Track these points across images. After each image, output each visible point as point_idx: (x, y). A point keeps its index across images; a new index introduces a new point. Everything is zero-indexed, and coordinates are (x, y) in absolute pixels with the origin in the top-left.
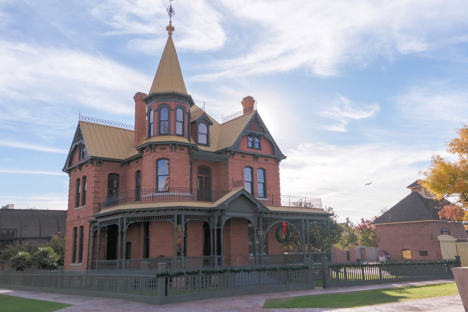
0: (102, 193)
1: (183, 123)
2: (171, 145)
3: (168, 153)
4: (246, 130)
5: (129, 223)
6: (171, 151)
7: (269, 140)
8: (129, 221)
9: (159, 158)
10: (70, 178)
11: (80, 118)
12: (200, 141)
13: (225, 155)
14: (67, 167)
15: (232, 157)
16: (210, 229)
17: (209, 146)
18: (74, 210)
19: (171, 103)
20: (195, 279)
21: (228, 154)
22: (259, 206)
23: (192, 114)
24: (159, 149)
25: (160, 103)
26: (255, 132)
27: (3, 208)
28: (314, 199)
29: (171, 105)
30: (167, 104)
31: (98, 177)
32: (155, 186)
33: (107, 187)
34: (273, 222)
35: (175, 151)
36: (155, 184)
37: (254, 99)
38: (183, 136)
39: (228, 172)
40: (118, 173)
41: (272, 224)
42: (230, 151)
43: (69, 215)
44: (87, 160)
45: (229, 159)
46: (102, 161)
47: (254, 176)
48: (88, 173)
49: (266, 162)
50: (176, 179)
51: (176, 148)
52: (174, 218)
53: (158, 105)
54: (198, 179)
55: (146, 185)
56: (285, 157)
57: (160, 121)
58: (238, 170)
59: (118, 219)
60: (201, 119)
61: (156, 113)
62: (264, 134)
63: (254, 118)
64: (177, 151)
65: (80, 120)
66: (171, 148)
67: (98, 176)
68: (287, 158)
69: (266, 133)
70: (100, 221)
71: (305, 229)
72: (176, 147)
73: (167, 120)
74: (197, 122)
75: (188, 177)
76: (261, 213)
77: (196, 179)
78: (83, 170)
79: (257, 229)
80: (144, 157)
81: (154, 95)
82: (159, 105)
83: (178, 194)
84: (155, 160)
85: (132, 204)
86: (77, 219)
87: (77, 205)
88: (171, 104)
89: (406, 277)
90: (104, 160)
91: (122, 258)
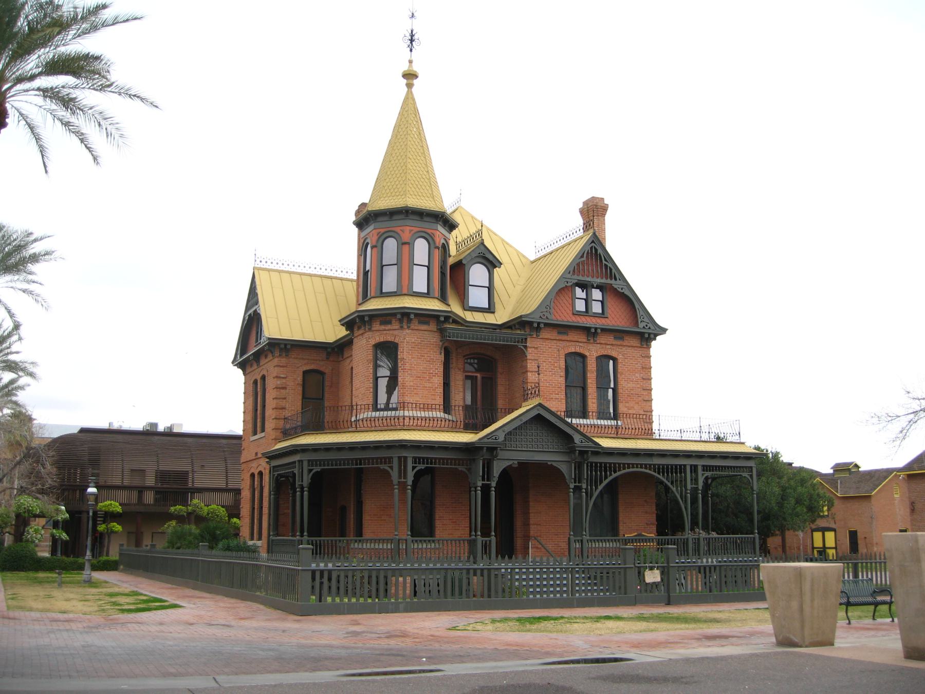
1: (428, 267)
2: (399, 316)
3: (396, 332)
4: (569, 276)
6: (402, 327)
7: (625, 295)
9: (379, 343)
11: (255, 261)
12: (472, 303)
13: (519, 332)
14: (239, 356)
15: (535, 336)
17: (492, 310)
21: (527, 330)
22: (577, 439)
25: (382, 231)
26: (589, 279)
29: (403, 232)
31: (283, 378)
32: (372, 398)
33: (300, 397)
34: (615, 472)
35: (409, 327)
36: (372, 394)
37: (581, 206)
38: (427, 295)
40: (322, 369)
41: (611, 475)
42: (530, 323)
43: (244, 449)
44: (264, 344)
45: (528, 340)
46: (289, 347)
47: (588, 373)
48: (267, 371)
50: (412, 384)
51: (409, 321)
52: (392, 463)
53: (378, 235)
54: (469, 383)
55: (357, 396)
56: (663, 331)
57: (382, 266)
58: (550, 362)
59: (294, 462)
60: (474, 255)
61: (375, 249)
62: (613, 282)
63: (588, 248)
64: (412, 327)
65: (256, 266)
66: (401, 321)
67: (282, 376)
68: (667, 332)
69: (616, 279)
70: (274, 465)
72: (411, 319)
73: (396, 263)
74: (464, 262)
75: (438, 380)
76: (582, 453)
77: (461, 383)
78: (261, 364)
79: (575, 486)
80: (355, 340)
81: (370, 215)
82: (380, 233)
84: (370, 347)
85: (319, 434)
86: (254, 458)
87: (255, 433)
89: (346, 600)
90: (292, 345)
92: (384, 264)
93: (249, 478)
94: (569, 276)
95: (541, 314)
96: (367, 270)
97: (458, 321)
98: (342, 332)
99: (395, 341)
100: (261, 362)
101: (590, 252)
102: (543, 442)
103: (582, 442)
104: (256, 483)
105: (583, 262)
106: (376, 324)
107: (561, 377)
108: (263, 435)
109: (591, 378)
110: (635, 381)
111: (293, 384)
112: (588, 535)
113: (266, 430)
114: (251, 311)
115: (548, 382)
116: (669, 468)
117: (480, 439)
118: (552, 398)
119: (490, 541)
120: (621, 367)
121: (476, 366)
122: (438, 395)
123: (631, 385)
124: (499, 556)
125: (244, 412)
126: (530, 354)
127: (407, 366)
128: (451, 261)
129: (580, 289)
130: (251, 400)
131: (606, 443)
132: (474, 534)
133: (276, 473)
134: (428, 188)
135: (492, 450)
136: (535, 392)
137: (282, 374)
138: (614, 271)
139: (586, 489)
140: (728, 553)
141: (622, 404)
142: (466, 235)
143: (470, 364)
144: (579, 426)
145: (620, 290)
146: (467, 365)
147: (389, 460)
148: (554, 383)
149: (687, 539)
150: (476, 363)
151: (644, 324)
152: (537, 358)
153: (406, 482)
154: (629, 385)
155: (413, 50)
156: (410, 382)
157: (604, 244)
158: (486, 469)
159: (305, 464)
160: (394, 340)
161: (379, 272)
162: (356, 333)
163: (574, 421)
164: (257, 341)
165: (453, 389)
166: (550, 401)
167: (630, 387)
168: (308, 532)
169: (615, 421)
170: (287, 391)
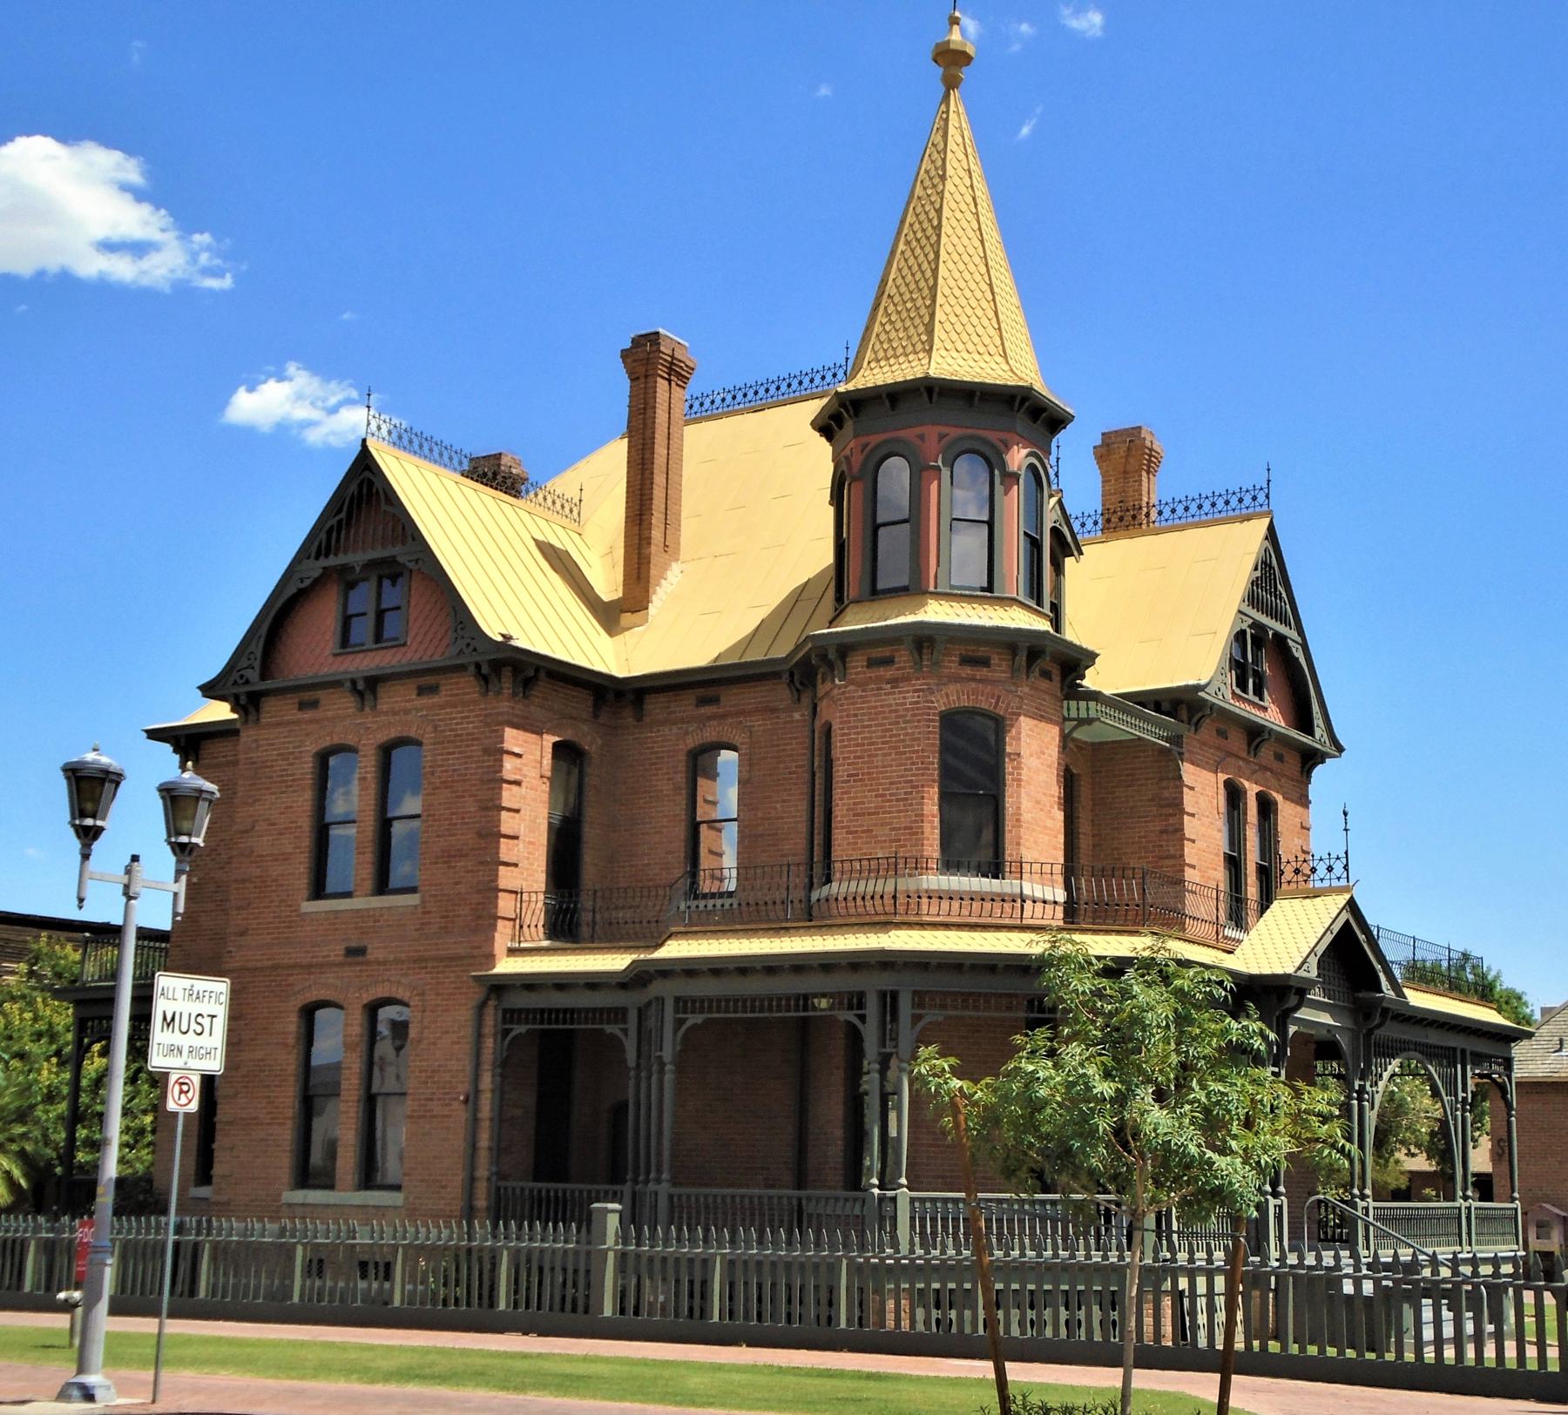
5: (512, 1030)
8: (511, 1022)
16: (672, 1076)
19: (918, 430)
25: (875, 439)
30: (898, 440)
57: (876, 528)
63: (353, 488)
82: (869, 447)
83: (890, 888)
88: (921, 437)
92: (880, 520)
99: (997, 711)
106: (949, 662)
157: (653, 572)
160: (995, 707)
161: (869, 545)
169: (500, 923)
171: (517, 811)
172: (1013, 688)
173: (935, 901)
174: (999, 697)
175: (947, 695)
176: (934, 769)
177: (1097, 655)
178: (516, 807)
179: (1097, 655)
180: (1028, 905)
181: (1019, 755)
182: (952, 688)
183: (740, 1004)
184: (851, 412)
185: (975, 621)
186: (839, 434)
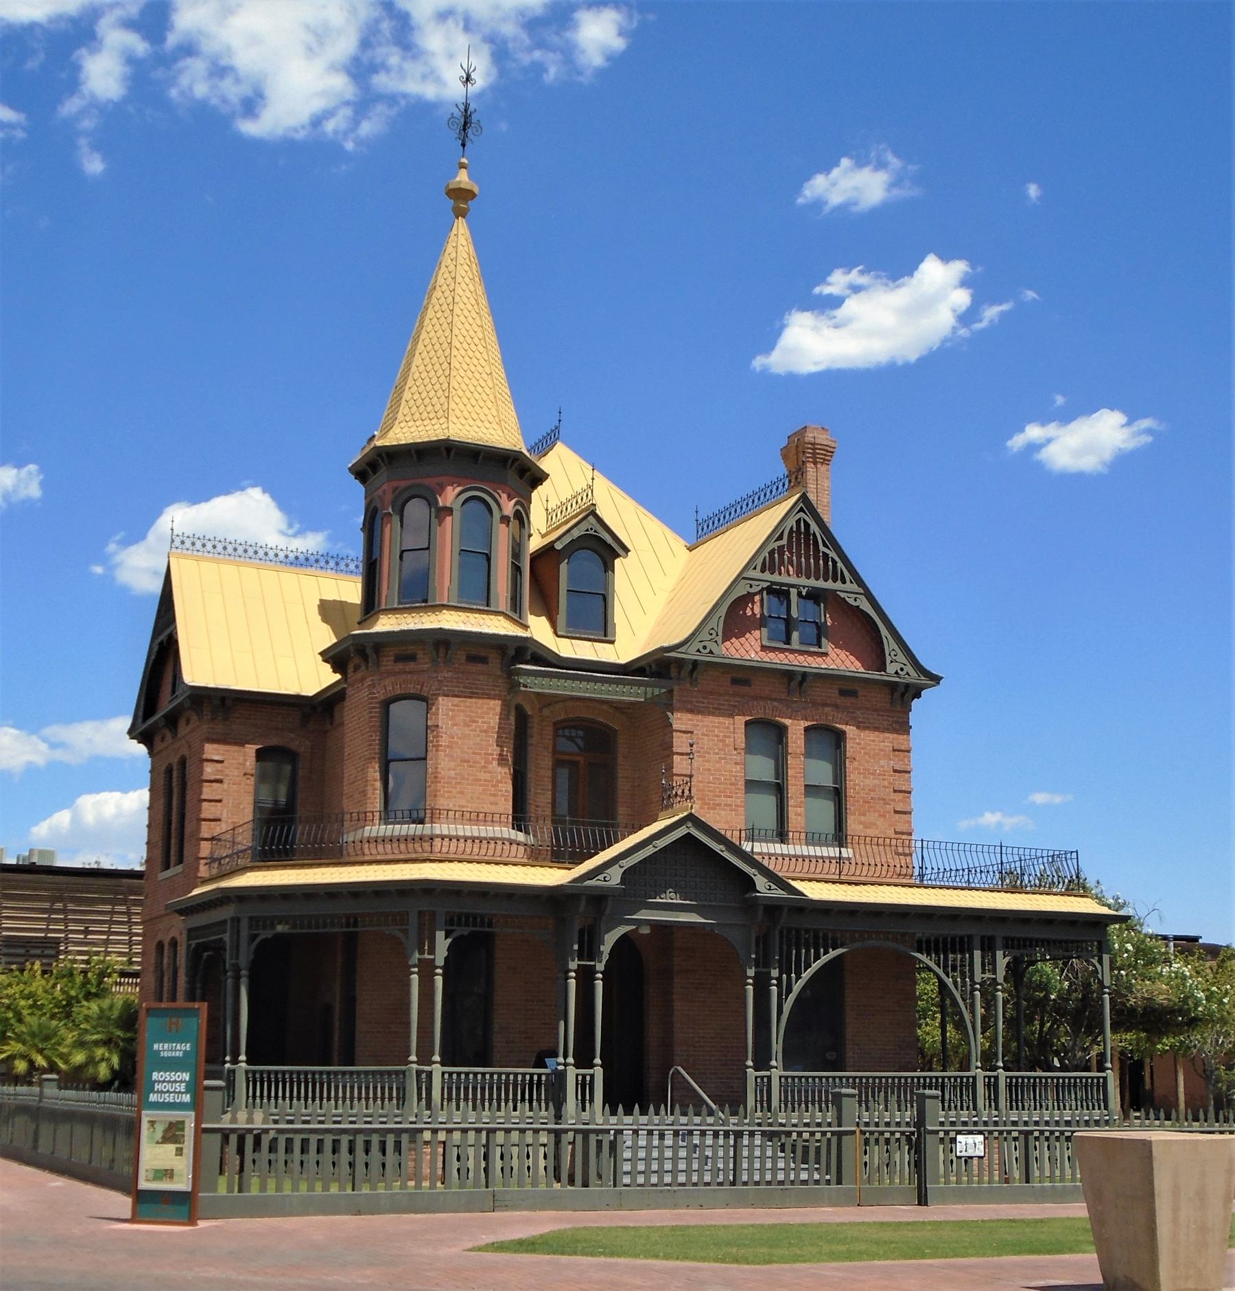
0: (230, 821)
4: (756, 574)
10: (152, 762)
11: (173, 541)
14: (140, 720)
18: (160, 879)
20: (305, 1150)
22: (761, 882)
23: (784, 485)
24: (392, 658)
25: (403, 484)
27: (21, 863)
28: (1039, 854)
37: (784, 443)
39: (670, 746)
49: (848, 701)
50: (452, 773)
52: (408, 924)
53: (394, 491)
54: (564, 773)
58: (718, 736)
59: (225, 922)
69: (844, 582)
71: (988, 975)
77: (549, 773)
84: (376, 703)
91: (425, 1058)
93: (154, 951)
94: (756, 574)
95: (700, 646)
96: (374, 558)
97: (541, 656)
98: (327, 677)
100: (179, 731)
101: (795, 529)
102: (656, 886)
103: (769, 889)
104: (165, 961)
105: (781, 548)
107: (736, 763)
108: (179, 868)
109: (795, 768)
110: (879, 775)
111: (236, 774)
112: (781, 1067)
113: (185, 860)
114: (163, 637)
115: (712, 774)
116: (955, 941)
117: (575, 880)
118: (719, 805)
119: (592, 1076)
120: (852, 747)
121: (579, 741)
122: (502, 795)
123: (870, 782)
124: (607, 1105)
125: (149, 826)
126: (143, 853)
127: (444, 741)
128: (535, 543)
129: (776, 599)
130: (161, 802)
131: (816, 891)
132: (563, 1061)
133: (193, 943)
134: (490, 405)
135: (599, 899)
136: (683, 792)
137: (218, 754)
138: (840, 565)
139: (779, 979)
140: (1041, 1106)
141: (852, 817)
142: (566, 494)
143: (570, 739)
144: (766, 857)
145: (851, 601)
146: (562, 740)
147: (401, 918)
148: (723, 775)
149: (974, 1078)
150: (580, 737)
151: (896, 667)
152: (689, 728)
153: (434, 959)
154: (867, 781)
155: (468, 144)
156: (449, 769)
158: (586, 938)
159: (244, 925)
160: (421, 691)
162: (352, 676)
163: (758, 847)
164: (173, 692)
165: (532, 785)
166: (715, 809)
167: (868, 785)
168: (247, 1054)
169: (750, 843)
170: (225, 786)
171: (220, 801)
172: (435, 675)
173: (373, 845)
174: (423, 683)
175: (385, 686)
176: (376, 745)
177: (942, 678)
178: (217, 798)
179: (942, 678)
180: (437, 842)
181: (437, 726)
182: (388, 682)
183: (261, 923)
184: (386, 462)
185: (412, 627)
186: (372, 478)
